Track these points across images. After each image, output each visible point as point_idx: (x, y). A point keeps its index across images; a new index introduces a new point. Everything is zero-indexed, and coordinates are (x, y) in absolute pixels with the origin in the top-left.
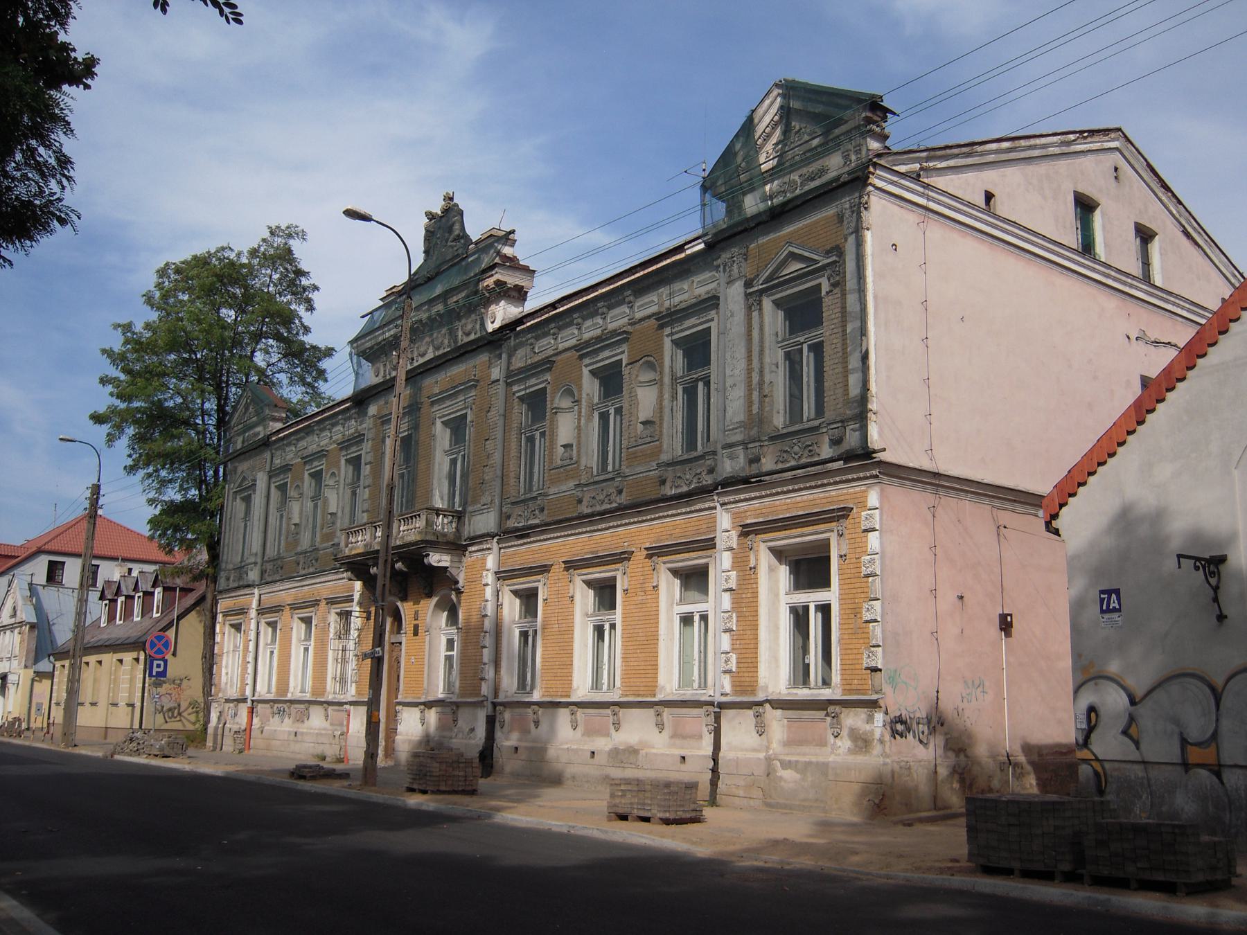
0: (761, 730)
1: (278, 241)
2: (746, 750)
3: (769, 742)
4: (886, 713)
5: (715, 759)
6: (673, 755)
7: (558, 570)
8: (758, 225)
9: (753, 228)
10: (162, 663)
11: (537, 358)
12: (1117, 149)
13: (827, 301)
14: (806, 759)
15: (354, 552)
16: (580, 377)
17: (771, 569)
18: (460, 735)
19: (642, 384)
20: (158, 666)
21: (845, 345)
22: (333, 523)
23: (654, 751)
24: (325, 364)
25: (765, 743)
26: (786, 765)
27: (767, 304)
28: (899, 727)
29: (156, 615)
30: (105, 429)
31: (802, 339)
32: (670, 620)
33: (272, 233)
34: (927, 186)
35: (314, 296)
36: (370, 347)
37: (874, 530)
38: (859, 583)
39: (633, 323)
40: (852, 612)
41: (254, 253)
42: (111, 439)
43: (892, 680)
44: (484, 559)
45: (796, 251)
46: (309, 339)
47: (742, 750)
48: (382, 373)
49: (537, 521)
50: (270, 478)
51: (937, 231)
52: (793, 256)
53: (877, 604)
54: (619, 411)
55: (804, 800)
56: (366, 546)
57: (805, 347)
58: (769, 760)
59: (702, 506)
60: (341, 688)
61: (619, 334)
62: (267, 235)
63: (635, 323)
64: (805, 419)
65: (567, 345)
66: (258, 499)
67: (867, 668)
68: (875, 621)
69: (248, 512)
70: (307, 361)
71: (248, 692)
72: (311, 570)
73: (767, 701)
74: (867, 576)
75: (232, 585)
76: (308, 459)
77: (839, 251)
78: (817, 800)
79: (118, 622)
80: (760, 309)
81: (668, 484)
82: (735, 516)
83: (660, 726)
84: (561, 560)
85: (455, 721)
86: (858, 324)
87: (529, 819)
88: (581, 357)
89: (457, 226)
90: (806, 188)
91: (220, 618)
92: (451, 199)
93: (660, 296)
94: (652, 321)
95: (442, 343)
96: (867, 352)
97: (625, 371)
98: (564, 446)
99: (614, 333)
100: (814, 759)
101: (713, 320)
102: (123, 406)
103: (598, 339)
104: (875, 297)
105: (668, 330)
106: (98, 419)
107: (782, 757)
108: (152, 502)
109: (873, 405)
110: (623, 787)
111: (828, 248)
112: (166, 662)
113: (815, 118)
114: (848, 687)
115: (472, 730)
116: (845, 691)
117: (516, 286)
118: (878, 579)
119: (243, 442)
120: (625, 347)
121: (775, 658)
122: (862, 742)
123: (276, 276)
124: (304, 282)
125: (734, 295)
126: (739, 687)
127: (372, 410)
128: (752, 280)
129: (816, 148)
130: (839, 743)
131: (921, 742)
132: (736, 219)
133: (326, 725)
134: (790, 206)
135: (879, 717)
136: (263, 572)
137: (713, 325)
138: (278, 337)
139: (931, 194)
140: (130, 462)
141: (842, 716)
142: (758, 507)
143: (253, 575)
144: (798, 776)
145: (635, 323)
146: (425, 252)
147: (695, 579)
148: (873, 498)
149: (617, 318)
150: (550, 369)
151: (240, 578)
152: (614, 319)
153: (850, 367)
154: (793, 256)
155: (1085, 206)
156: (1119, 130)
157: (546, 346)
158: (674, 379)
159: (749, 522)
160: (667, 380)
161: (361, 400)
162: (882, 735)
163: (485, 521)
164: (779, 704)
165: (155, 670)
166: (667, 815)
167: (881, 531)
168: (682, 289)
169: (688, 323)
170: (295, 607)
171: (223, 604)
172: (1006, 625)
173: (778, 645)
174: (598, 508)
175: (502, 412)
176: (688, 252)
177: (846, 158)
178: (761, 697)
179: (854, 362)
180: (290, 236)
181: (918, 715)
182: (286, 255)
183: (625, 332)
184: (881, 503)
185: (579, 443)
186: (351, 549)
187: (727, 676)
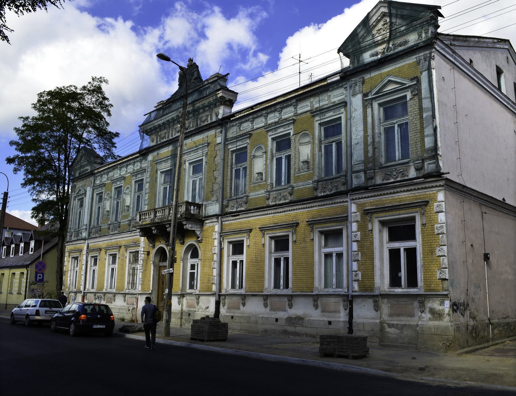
0: (377, 308)
1: (96, 83)
2: (368, 319)
3: (381, 315)
4: (450, 301)
5: (350, 321)
6: (324, 321)
7: (256, 232)
8: (370, 67)
9: (368, 69)
10: (41, 275)
11: (241, 133)
12: (507, 49)
13: (409, 104)
14: (403, 323)
15: (144, 223)
16: (267, 141)
17: (380, 231)
18: (201, 310)
19: (301, 144)
20: (40, 276)
21: (422, 124)
22: (128, 210)
23: (312, 318)
24: (115, 140)
25: (379, 315)
26: (390, 326)
27: (375, 105)
28: (455, 307)
29: (30, 253)
30: (12, 166)
31: (395, 121)
32: (320, 256)
33: (93, 79)
34: (454, 52)
35: (110, 109)
36: (146, 129)
37: (442, 212)
38: (431, 238)
39: (296, 115)
40: (430, 251)
41: (84, 88)
42: (16, 170)
43: (452, 284)
44: (213, 227)
45: (393, 79)
46: (110, 129)
47: (366, 319)
48: (155, 141)
49: (243, 209)
50: (93, 190)
51: (458, 75)
52: (390, 82)
53: (445, 248)
54: (288, 158)
55: (402, 343)
56: (151, 220)
57: (396, 126)
58: (381, 323)
59: (339, 201)
60: (132, 287)
61: (289, 120)
62: (91, 80)
63: (297, 115)
64: (397, 159)
65: (258, 126)
66: (87, 200)
67: (439, 279)
68: (444, 256)
69: (81, 205)
70: (108, 138)
71: (82, 288)
72: (116, 232)
73: (381, 295)
74: (439, 234)
75: (73, 239)
76: (114, 181)
77: (418, 79)
78: (409, 343)
79: (11, 256)
80: (372, 108)
81: (319, 191)
82: (358, 206)
83: (266, 306)
84: (259, 227)
85: (198, 303)
86: (430, 113)
87: (275, 356)
88: (268, 131)
89: (196, 73)
90: (396, 50)
91: (67, 254)
92: (192, 61)
93: (311, 103)
94: (309, 114)
95: (189, 126)
96: (436, 127)
97: (292, 138)
98: (257, 173)
99: (286, 120)
100: (407, 323)
101: (343, 113)
102: (21, 155)
103: (276, 123)
104: (438, 101)
105: (317, 118)
106: (10, 161)
107: (388, 322)
108: (34, 200)
109: (440, 152)
110: (328, 340)
111: (412, 77)
112: (43, 274)
113: (402, 17)
114: (428, 288)
115: (208, 308)
116: (426, 290)
117: (229, 99)
118: (445, 236)
119: (79, 173)
120: (292, 126)
121: (382, 274)
122: (437, 315)
123: (94, 99)
124: (107, 102)
125: (357, 101)
126: (362, 287)
127: (150, 157)
128: (368, 93)
129: (403, 31)
130: (423, 315)
131: (462, 314)
132: (356, 65)
133: (125, 304)
134: (389, 58)
135: (447, 303)
136: (89, 233)
137: (343, 116)
138: (94, 127)
139: (456, 57)
140: (23, 182)
141: (425, 302)
142: (370, 201)
143: (84, 234)
144: (398, 331)
145: (297, 115)
146: (179, 85)
147: (333, 236)
148: (441, 196)
149: (288, 113)
150: (250, 137)
151: (78, 236)
152: (285, 113)
153: (426, 134)
154: (390, 82)
155: (499, 72)
156: (508, 41)
157: (247, 126)
158: (320, 142)
159: (367, 208)
160: (317, 142)
161: (144, 153)
162: (449, 312)
163: (214, 208)
164: (384, 296)
165: (38, 278)
166: (356, 354)
167: (446, 212)
168: (325, 99)
169: (328, 115)
170: (107, 249)
171: (68, 247)
172: (486, 257)
173: (383, 267)
174: (278, 202)
175: (222, 157)
176: (329, 81)
177: (420, 36)
178: (377, 293)
179: (429, 131)
180: (101, 82)
181: (460, 301)
182: (98, 90)
183: (293, 119)
184: (445, 199)
185: (266, 172)
186: (143, 222)
187: (356, 283)
